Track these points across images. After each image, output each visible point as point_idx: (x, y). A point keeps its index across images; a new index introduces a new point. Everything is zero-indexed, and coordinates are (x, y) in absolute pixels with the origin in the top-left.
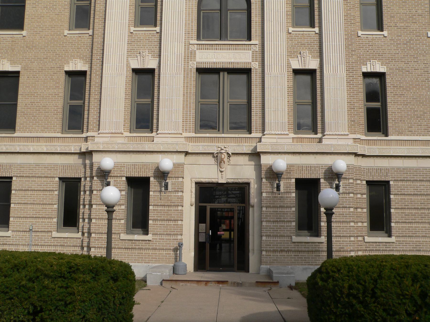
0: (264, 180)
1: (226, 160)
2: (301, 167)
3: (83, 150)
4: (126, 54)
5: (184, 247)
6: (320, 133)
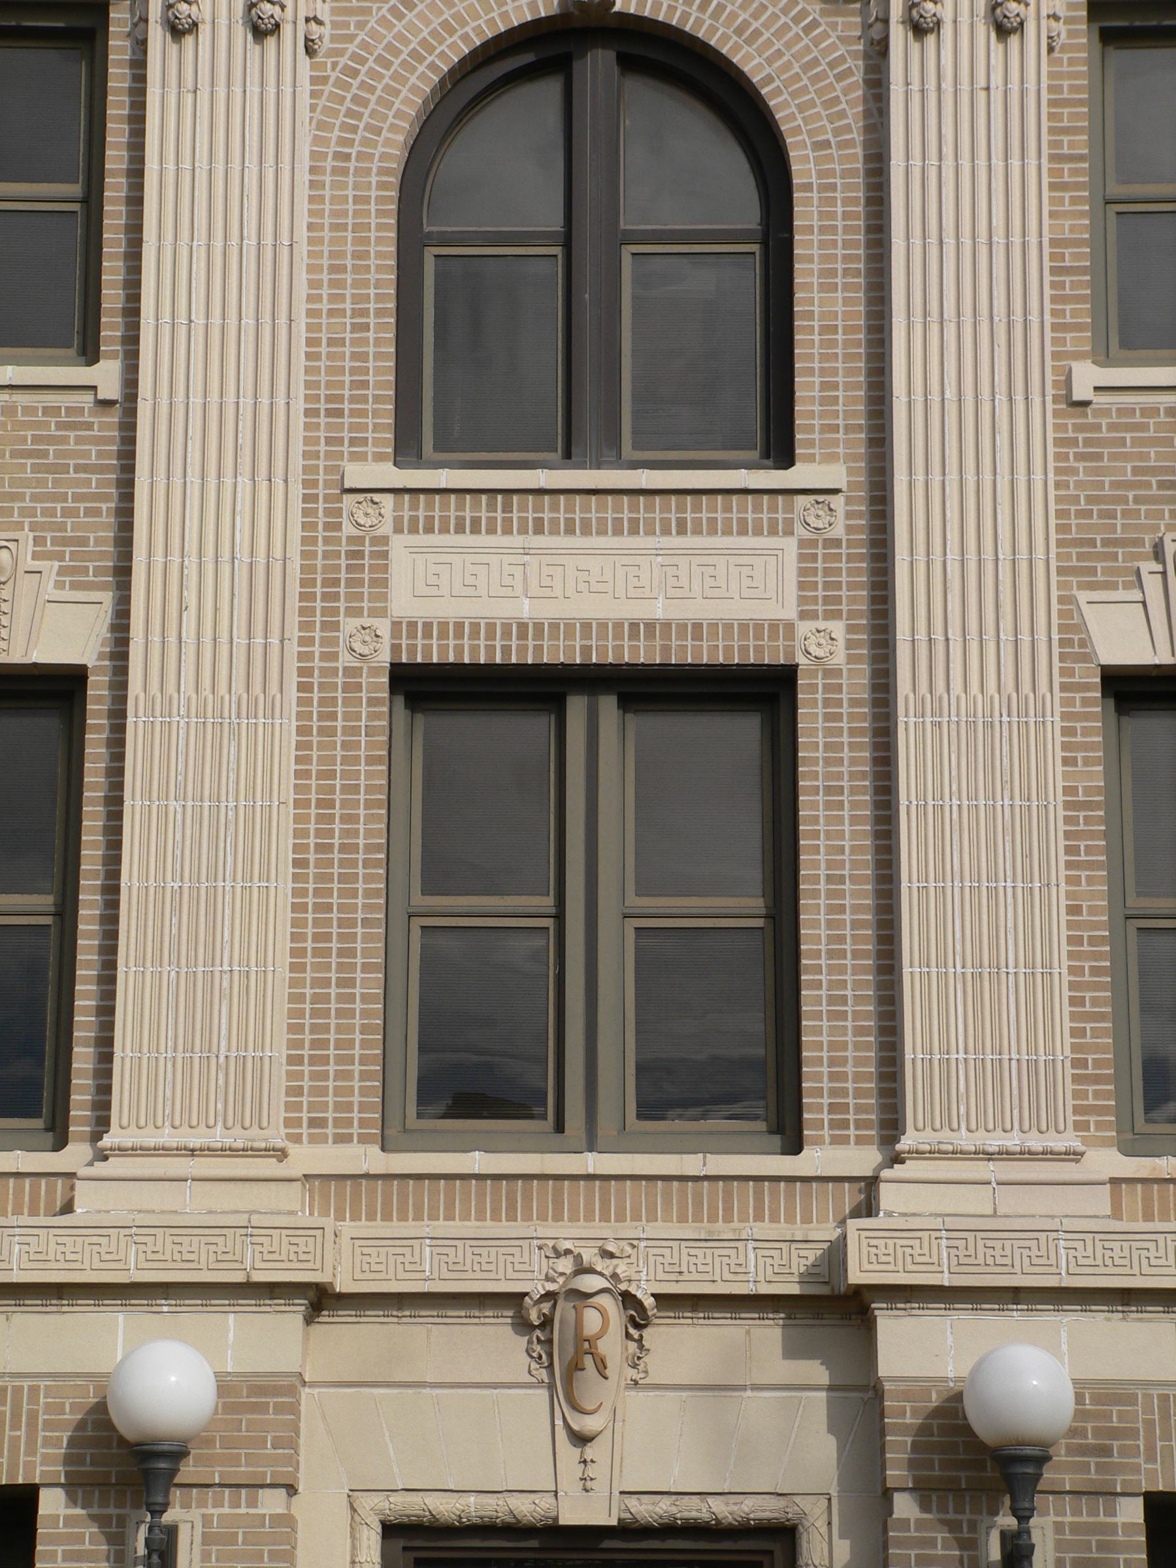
6: (81, 1138)
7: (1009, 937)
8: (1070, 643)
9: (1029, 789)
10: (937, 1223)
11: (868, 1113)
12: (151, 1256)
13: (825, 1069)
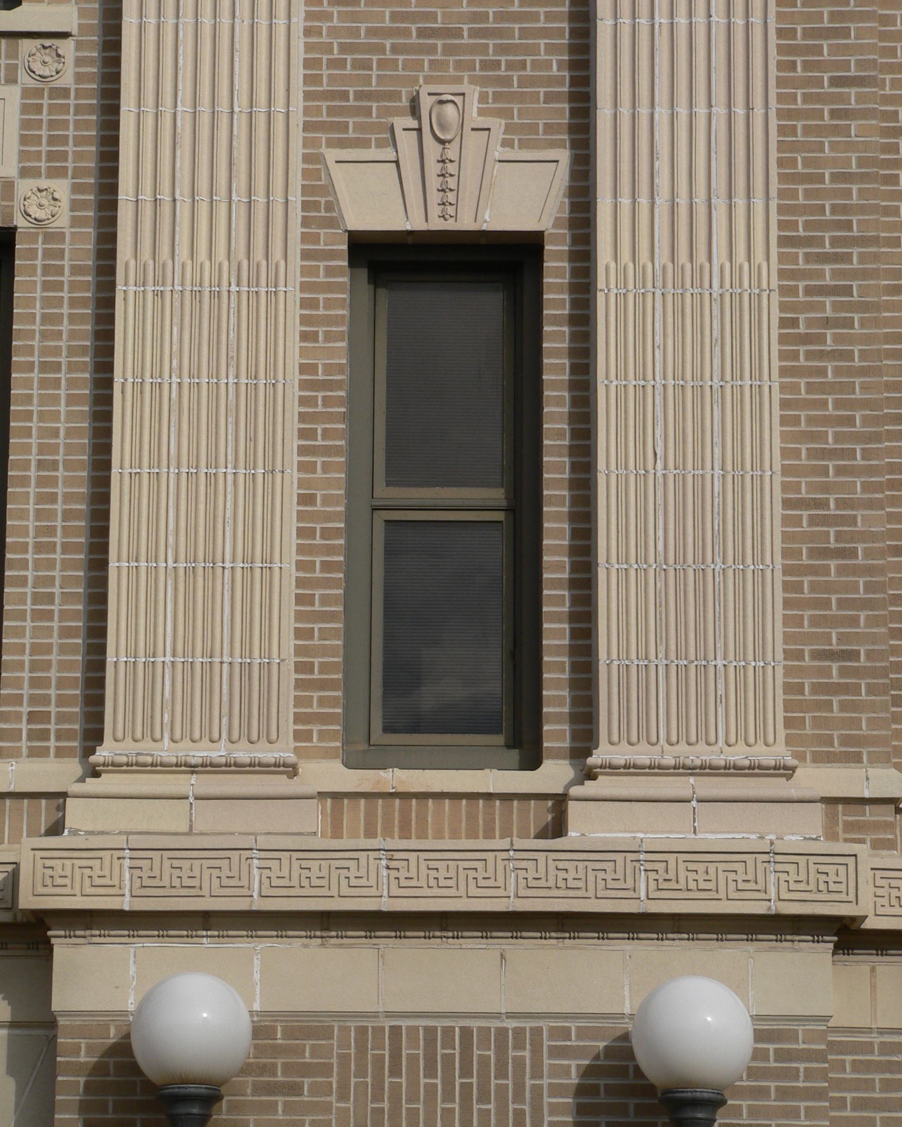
6: (557, 754)
7: (227, 528)
8: (315, 206)
9: (256, 366)
10: (120, 841)
11: (70, 722)
12: (225, 882)
13: (26, 675)
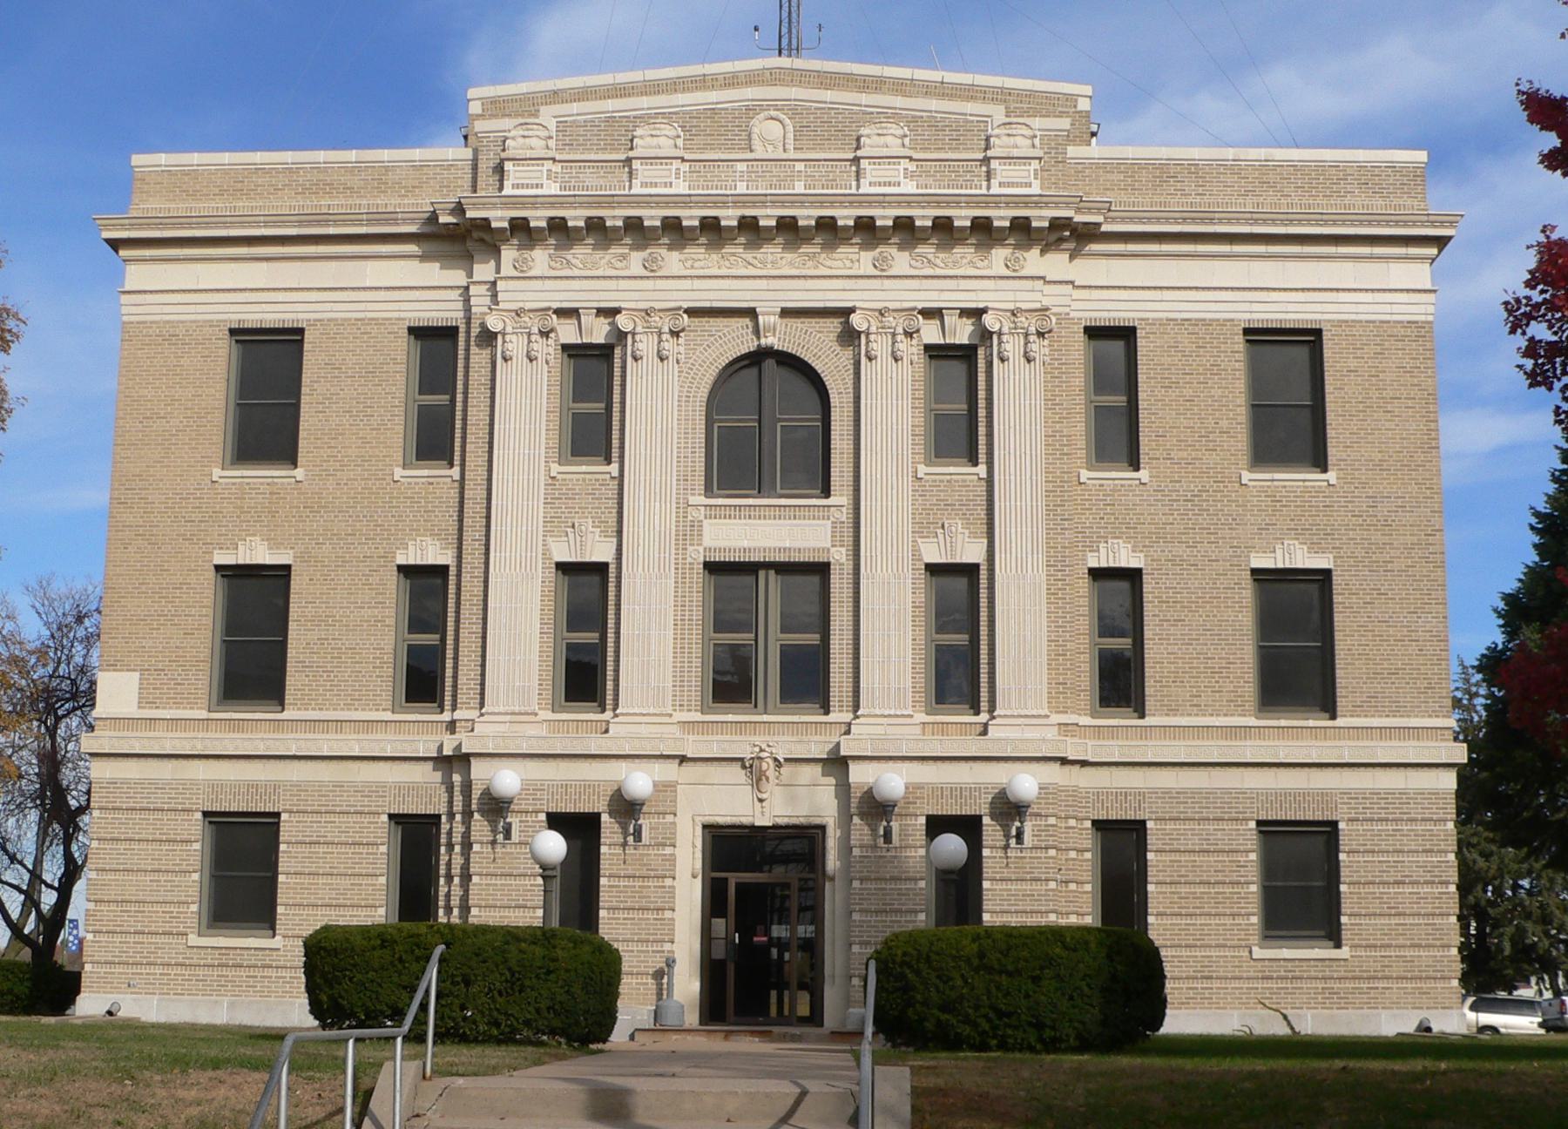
0: (856, 820)
1: (771, 773)
2: (939, 791)
3: (447, 751)
4: (541, 529)
5: (676, 969)
